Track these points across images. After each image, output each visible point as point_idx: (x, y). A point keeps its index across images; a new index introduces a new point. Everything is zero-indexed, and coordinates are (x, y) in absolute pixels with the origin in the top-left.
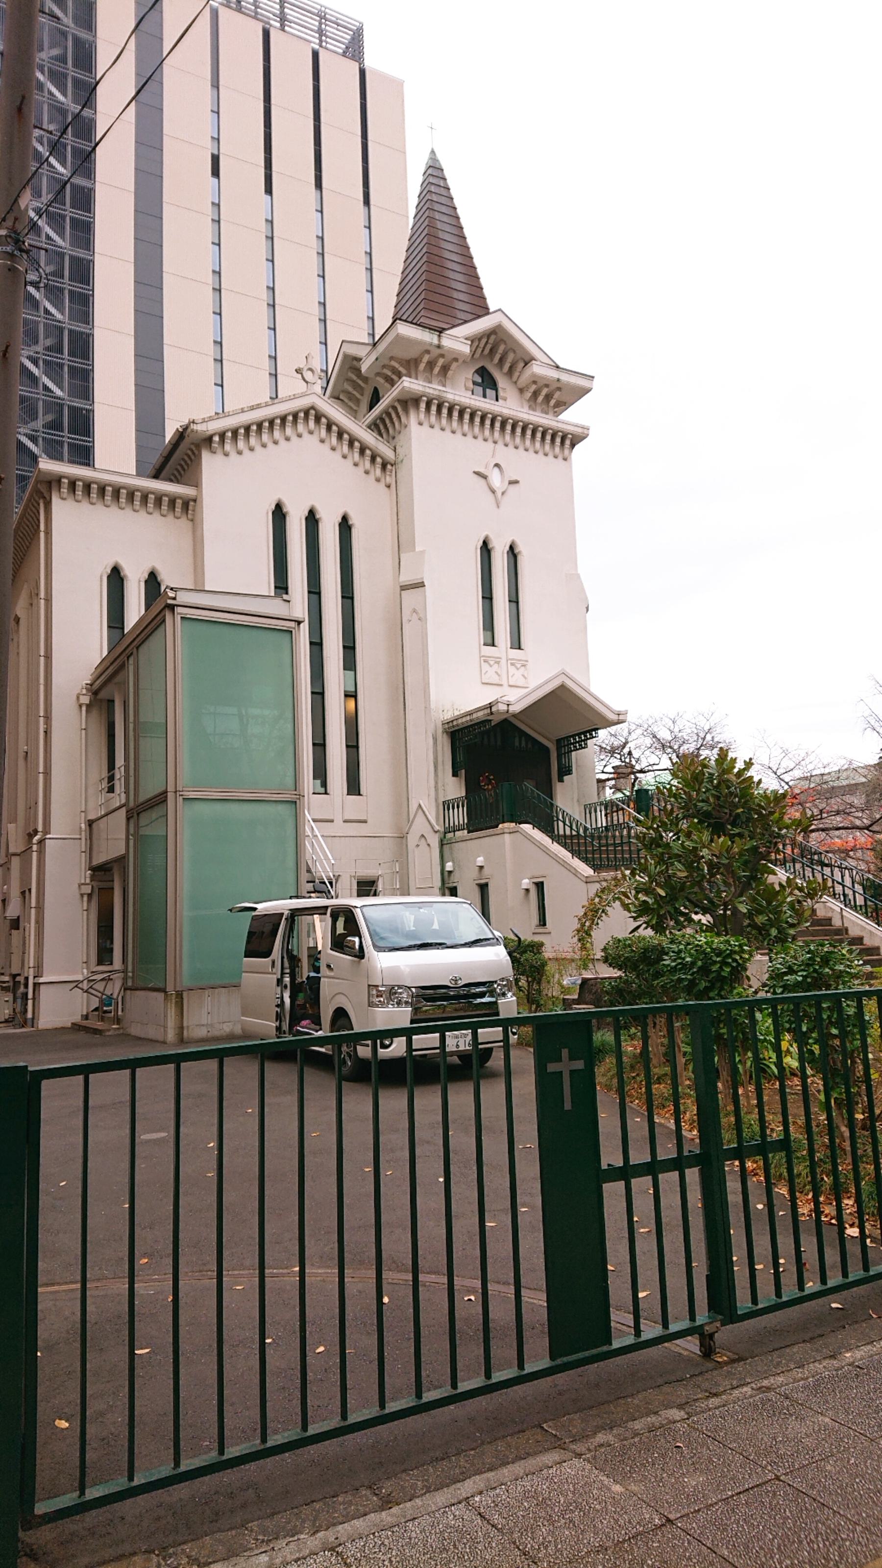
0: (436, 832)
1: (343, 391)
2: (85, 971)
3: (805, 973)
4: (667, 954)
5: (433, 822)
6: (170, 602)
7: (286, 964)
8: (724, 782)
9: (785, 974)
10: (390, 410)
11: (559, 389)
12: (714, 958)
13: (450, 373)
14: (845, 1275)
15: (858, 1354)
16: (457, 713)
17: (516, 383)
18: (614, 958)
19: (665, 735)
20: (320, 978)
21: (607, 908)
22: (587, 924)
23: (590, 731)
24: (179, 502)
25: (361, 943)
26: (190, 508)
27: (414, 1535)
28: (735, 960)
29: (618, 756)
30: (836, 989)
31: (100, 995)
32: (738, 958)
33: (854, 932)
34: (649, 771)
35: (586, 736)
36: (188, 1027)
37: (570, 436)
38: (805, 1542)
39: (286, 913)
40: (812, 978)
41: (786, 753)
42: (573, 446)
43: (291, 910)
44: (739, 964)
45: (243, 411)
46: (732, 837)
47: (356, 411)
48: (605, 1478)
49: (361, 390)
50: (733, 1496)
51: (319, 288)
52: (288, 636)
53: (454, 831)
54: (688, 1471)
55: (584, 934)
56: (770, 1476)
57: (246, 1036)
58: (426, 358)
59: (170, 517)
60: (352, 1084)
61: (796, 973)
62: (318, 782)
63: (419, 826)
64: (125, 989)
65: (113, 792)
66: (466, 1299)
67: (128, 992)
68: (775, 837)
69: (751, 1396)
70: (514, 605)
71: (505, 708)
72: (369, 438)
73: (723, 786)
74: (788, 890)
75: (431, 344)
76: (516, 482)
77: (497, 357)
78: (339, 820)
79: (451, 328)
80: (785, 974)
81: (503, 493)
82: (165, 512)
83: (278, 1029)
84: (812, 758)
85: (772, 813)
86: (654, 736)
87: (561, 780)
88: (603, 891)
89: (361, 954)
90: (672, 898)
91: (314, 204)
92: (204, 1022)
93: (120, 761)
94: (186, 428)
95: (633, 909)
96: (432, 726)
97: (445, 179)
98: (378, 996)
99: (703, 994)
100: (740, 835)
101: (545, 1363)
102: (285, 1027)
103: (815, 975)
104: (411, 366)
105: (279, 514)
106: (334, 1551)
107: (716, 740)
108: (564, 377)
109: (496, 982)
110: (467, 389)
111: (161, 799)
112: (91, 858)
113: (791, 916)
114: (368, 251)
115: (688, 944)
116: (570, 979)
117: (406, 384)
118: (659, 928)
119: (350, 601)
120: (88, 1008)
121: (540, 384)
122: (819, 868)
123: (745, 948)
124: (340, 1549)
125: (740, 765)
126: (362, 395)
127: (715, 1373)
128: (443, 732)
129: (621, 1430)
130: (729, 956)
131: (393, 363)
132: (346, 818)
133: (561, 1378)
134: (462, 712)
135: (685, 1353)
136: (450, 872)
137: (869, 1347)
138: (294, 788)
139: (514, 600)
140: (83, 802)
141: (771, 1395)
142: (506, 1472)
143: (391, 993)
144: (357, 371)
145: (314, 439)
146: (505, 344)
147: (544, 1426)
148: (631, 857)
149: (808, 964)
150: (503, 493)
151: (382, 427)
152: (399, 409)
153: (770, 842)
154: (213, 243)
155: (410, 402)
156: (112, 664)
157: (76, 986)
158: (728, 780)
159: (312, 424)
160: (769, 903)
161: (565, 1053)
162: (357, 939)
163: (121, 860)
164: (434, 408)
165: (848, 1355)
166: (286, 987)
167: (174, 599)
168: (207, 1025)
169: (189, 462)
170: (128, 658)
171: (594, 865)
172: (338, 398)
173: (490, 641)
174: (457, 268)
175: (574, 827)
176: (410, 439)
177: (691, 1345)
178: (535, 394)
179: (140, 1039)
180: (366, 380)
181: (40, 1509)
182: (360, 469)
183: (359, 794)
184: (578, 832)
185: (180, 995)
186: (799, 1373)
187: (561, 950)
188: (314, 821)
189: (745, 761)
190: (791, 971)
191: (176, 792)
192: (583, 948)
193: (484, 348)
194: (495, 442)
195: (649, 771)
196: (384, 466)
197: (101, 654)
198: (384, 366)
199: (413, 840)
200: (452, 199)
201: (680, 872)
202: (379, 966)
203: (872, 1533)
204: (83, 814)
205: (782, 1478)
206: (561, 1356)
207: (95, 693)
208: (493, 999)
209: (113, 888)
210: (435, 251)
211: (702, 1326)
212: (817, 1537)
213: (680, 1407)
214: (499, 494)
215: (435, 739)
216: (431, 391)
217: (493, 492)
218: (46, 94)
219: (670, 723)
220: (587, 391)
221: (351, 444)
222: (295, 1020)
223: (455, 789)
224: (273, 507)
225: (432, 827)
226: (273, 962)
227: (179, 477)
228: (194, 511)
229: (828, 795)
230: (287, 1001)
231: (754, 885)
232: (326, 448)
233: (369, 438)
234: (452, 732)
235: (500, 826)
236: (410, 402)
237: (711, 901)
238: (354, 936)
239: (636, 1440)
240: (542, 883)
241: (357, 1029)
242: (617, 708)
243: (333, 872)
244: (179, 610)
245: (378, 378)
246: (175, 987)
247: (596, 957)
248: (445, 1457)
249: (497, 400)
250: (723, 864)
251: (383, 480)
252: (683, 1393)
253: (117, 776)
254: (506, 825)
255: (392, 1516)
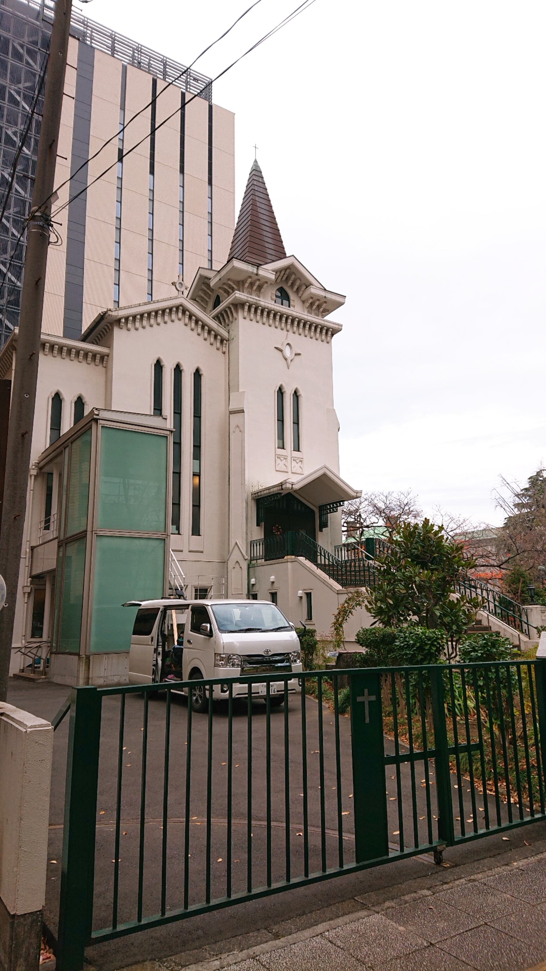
0: (246, 560)
1: (198, 296)
2: (23, 641)
3: (482, 652)
4: (397, 638)
5: (244, 553)
6: (95, 417)
7: (160, 640)
8: (426, 538)
9: (471, 652)
10: (227, 309)
11: (325, 302)
12: (427, 642)
13: (263, 290)
14: (511, 821)
15: (521, 864)
16: (260, 488)
17: (300, 297)
18: (363, 640)
19: (382, 505)
20: (182, 649)
21: (352, 610)
22: (340, 619)
23: (339, 502)
24: (98, 356)
25: (211, 627)
26: (105, 360)
27: (296, 951)
28: (439, 643)
29: (353, 517)
30: (499, 660)
31: (33, 656)
32: (440, 642)
33: (494, 629)
34: (372, 527)
35: (337, 505)
36: (92, 678)
37: (331, 330)
38: (504, 954)
39: (162, 608)
40: (486, 654)
41: (452, 519)
42: (332, 335)
43: (164, 606)
44: (440, 646)
45: (140, 305)
46: (432, 570)
47: (205, 308)
48: (394, 923)
49: (209, 296)
50: (463, 932)
51: (180, 231)
52: (165, 439)
53: (257, 560)
54: (438, 920)
55: (338, 626)
56: (482, 923)
57: (131, 683)
58: (249, 281)
59: (93, 365)
60: (201, 714)
61: (477, 651)
62: (175, 527)
63: (235, 556)
64: (51, 653)
65: (49, 529)
66: (297, 834)
67: (53, 655)
68: (456, 571)
69: (466, 884)
70: (296, 425)
71: (290, 486)
72: (214, 324)
73: (426, 541)
74: (462, 603)
75: (252, 273)
76: (299, 354)
77: (290, 282)
78: (186, 550)
79: (265, 264)
80: (471, 652)
81: (291, 361)
82: (89, 362)
83: (154, 680)
84: (467, 522)
85: (455, 557)
86: (375, 506)
87: (321, 530)
88: (350, 599)
89: (210, 634)
90: (396, 606)
91: (178, 182)
92: (102, 675)
93: (54, 510)
94: (105, 313)
95: (372, 611)
96: (246, 494)
97: (262, 178)
98: (220, 660)
99: (421, 662)
100: (436, 569)
101: (353, 865)
102: (158, 678)
103: (488, 653)
104: (240, 284)
105: (158, 366)
106: (254, 959)
107: (411, 509)
108: (329, 296)
109: (291, 653)
110: (272, 299)
111: (81, 536)
112: (31, 570)
113: (464, 619)
114: (210, 211)
115: (411, 633)
116: (331, 653)
117: (237, 295)
118: (387, 623)
119: (199, 419)
120: (24, 664)
121: (315, 298)
122: (474, 590)
123: (444, 636)
124: (258, 958)
125: (436, 528)
126: (209, 299)
127: (444, 872)
128: (252, 499)
129: (398, 900)
130: (435, 641)
131: (230, 282)
132: (191, 549)
133: (360, 874)
134: (263, 488)
135: (426, 862)
136: (253, 585)
137: (526, 860)
138: (163, 530)
139: (296, 422)
140: (29, 535)
141: (476, 883)
142: (340, 921)
143: (228, 659)
144: (208, 286)
145: (181, 323)
146: (295, 275)
147: (356, 898)
148: (365, 579)
149: (484, 646)
150: (291, 361)
151: (221, 319)
152: (232, 309)
153: (453, 574)
154: (117, 201)
155: (239, 305)
156: (53, 451)
157: (19, 651)
158: (429, 537)
159: (180, 314)
160: (452, 610)
161: (366, 691)
162: (208, 625)
163: (52, 572)
164: (253, 310)
165: (515, 864)
166: (159, 654)
167: (98, 415)
168: (104, 677)
169: (105, 333)
170: (65, 449)
171: (342, 583)
172: (195, 300)
173: (281, 446)
174: (268, 229)
175: (331, 560)
176: (238, 327)
177: (428, 859)
178: (312, 304)
179: (60, 685)
180: (212, 290)
181: (94, 935)
182: (208, 342)
183: (199, 535)
184: (333, 563)
185: (88, 658)
186: (490, 873)
187: (324, 635)
188: (173, 551)
189: (439, 526)
190: (474, 650)
191: (92, 531)
192: (338, 634)
193: (283, 276)
194: (288, 331)
195: (372, 527)
196: (222, 342)
197: (46, 445)
198: (224, 284)
199: (231, 564)
200: (266, 189)
201: (401, 589)
202: (222, 642)
203: (538, 950)
204: (28, 542)
205: (488, 924)
206: (362, 861)
207: (41, 469)
208: (288, 664)
209: (45, 589)
210: (255, 219)
211: (436, 847)
212: (510, 951)
213: (428, 889)
214: (289, 361)
215: (247, 503)
216: (252, 300)
217: (286, 359)
218: (21, 108)
219: (384, 498)
220: (342, 304)
221: (203, 327)
222: (164, 674)
223: (258, 534)
224: (155, 362)
225: (243, 556)
226: (152, 638)
227: (98, 341)
228: (107, 362)
229: (476, 545)
230: (160, 662)
231: (443, 599)
232: (188, 329)
233: (214, 324)
234: (257, 499)
235: (286, 557)
236: (239, 305)
237: (418, 608)
238: (207, 623)
239: (407, 905)
240: (310, 593)
241: (206, 678)
242: (356, 488)
243: (184, 583)
244: (100, 422)
245: (220, 290)
246: (85, 652)
247: (345, 640)
248: (304, 913)
249: (289, 307)
250: (427, 586)
251: (221, 349)
252: (428, 882)
253: (52, 520)
254: (289, 557)
255: (282, 942)
